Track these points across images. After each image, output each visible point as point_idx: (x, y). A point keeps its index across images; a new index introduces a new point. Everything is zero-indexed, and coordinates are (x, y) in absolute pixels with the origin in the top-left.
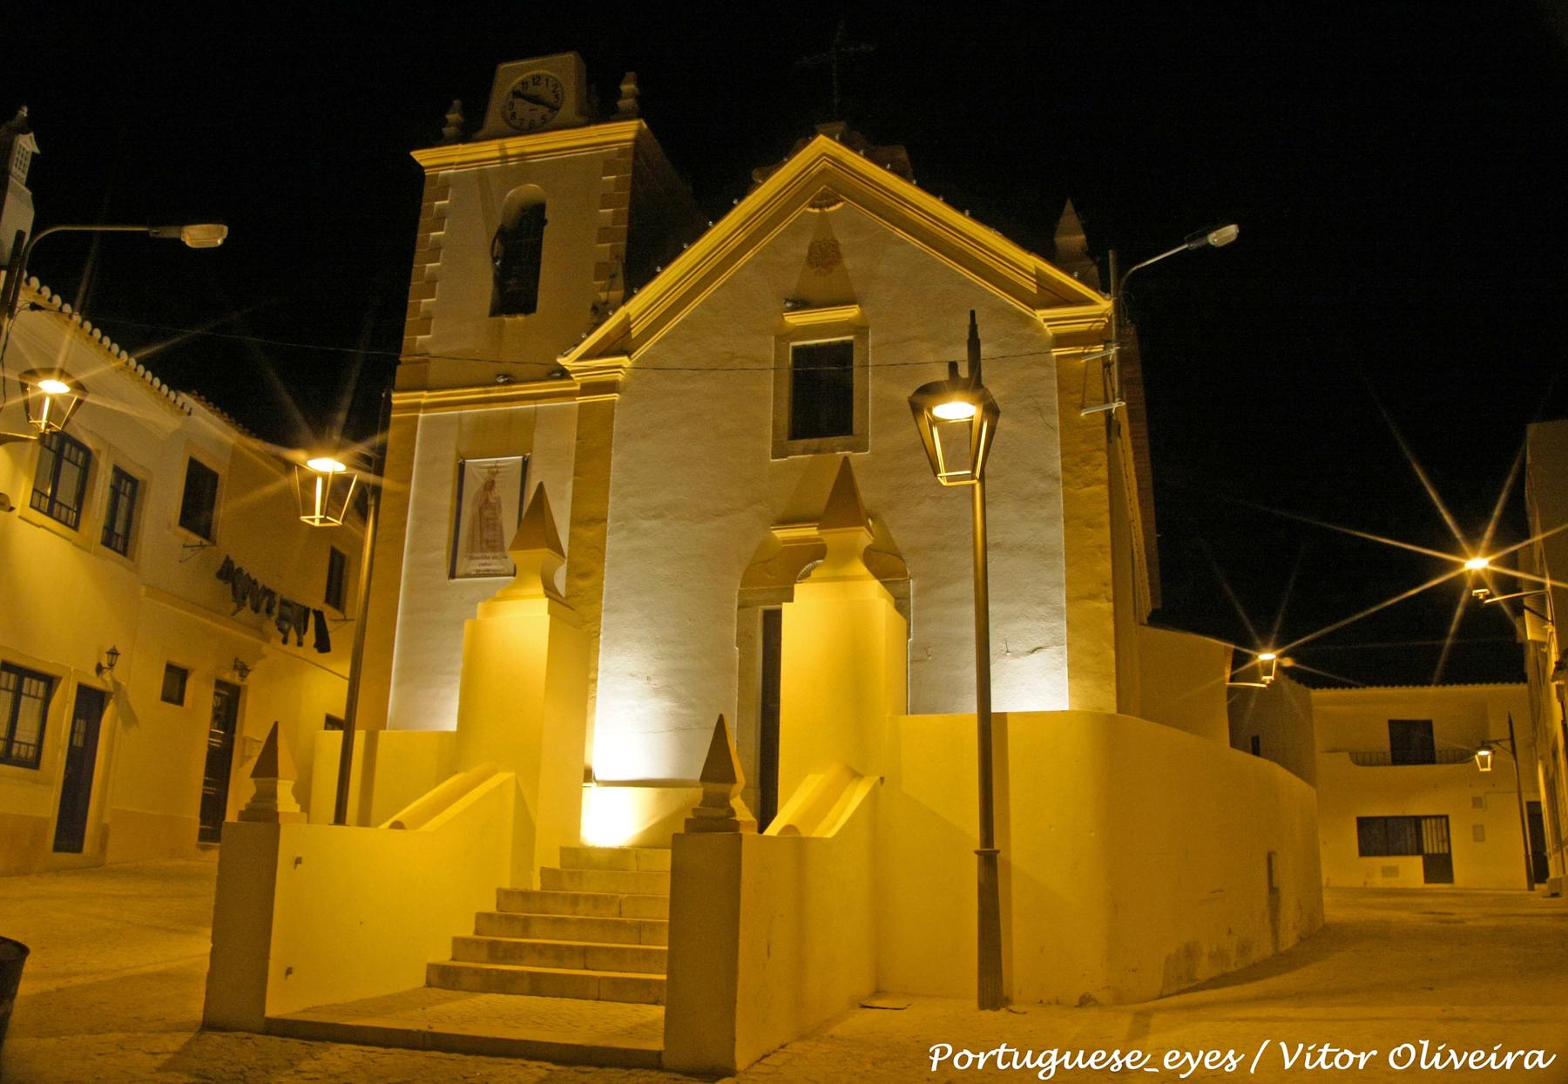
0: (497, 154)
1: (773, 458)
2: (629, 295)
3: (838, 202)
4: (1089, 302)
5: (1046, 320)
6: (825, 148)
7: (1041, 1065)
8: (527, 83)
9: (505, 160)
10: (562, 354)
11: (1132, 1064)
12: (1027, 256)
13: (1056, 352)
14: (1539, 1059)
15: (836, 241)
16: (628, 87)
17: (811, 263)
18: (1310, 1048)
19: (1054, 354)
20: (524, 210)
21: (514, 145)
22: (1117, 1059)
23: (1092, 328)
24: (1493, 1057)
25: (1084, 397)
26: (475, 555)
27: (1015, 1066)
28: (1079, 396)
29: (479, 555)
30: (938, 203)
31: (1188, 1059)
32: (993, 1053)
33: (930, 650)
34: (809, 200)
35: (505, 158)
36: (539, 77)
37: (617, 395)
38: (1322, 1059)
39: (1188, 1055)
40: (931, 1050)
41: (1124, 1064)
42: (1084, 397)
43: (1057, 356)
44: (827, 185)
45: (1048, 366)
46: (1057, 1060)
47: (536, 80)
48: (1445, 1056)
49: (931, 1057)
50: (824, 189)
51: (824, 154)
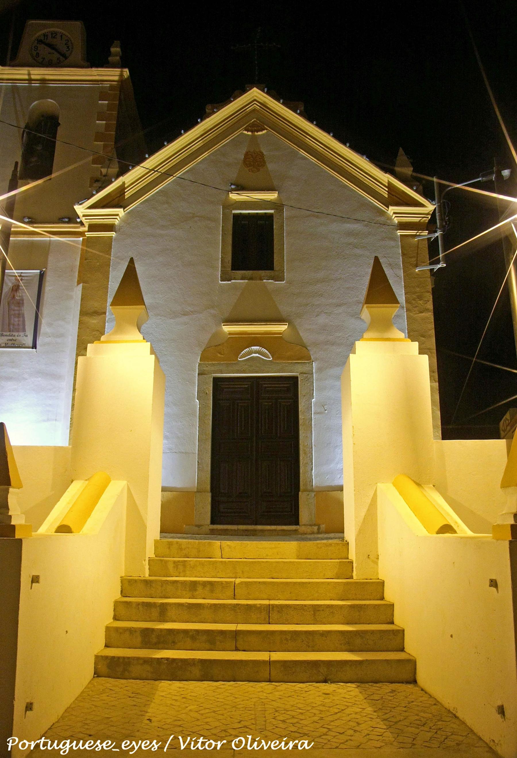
0: (26, 77)
1: (221, 281)
2: (123, 171)
3: (264, 130)
4: (422, 205)
5: (394, 213)
6: (256, 96)
7: (62, 748)
8: (47, 36)
9: (30, 82)
10: (79, 203)
11: (107, 747)
12: (384, 174)
13: (399, 233)
14: (306, 745)
15: (262, 153)
16: (116, 50)
17: (246, 164)
18: (193, 739)
19: (399, 234)
20: (43, 116)
21: (37, 73)
22: (99, 745)
23: (421, 221)
24: (283, 744)
25: (417, 260)
26: (5, 333)
27: (49, 748)
28: (414, 259)
29: (8, 333)
30: (329, 137)
31: (133, 745)
32: (38, 741)
33: (325, 407)
34: (245, 126)
35: (30, 80)
36: (56, 33)
37: (114, 233)
38: (199, 745)
39: (134, 743)
40: (8, 740)
41: (102, 747)
42: (417, 260)
43: (400, 235)
44: (257, 119)
45: (395, 240)
46: (69, 745)
47: (54, 35)
48: (259, 743)
49: (8, 744)
50: (255, 121)
51: (255, 100)
